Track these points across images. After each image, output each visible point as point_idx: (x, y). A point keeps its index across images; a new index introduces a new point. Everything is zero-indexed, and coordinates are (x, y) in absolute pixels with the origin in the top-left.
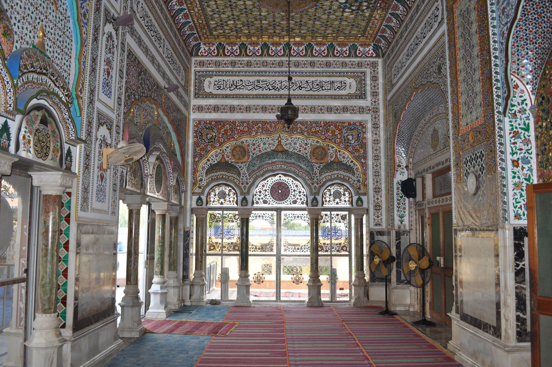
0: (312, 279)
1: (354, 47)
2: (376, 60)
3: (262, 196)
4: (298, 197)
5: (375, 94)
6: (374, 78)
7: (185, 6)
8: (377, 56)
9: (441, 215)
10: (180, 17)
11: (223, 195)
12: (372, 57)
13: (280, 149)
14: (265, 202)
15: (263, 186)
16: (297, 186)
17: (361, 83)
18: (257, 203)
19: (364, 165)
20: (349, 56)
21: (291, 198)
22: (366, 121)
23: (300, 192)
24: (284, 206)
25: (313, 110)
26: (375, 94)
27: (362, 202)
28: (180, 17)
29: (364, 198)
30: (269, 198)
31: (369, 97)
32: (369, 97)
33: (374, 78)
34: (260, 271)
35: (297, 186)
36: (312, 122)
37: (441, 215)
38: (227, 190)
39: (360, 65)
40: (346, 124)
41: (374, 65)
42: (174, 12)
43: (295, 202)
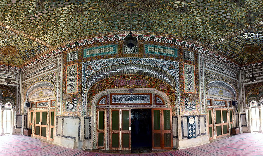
0: (171, 143)
1: (16, 68)
2: (20, 72)
5: (242, 87)
6: (19, 77)
8: (21, 71)
9: (120, 143)
11: (253, 103)
12: (19, 71)
17: (16, 77)
19: (16, 98)
20: (14, 70)
22: (17, 87)
26: (242, 87)
29: (15, 106)
31: (244, 86)
32: (244, 86)
33: (19, 77)
34: (2, 111)
37: (120, 143)
38: (254, 101)
39: (16, 72)
41: (20, 73)
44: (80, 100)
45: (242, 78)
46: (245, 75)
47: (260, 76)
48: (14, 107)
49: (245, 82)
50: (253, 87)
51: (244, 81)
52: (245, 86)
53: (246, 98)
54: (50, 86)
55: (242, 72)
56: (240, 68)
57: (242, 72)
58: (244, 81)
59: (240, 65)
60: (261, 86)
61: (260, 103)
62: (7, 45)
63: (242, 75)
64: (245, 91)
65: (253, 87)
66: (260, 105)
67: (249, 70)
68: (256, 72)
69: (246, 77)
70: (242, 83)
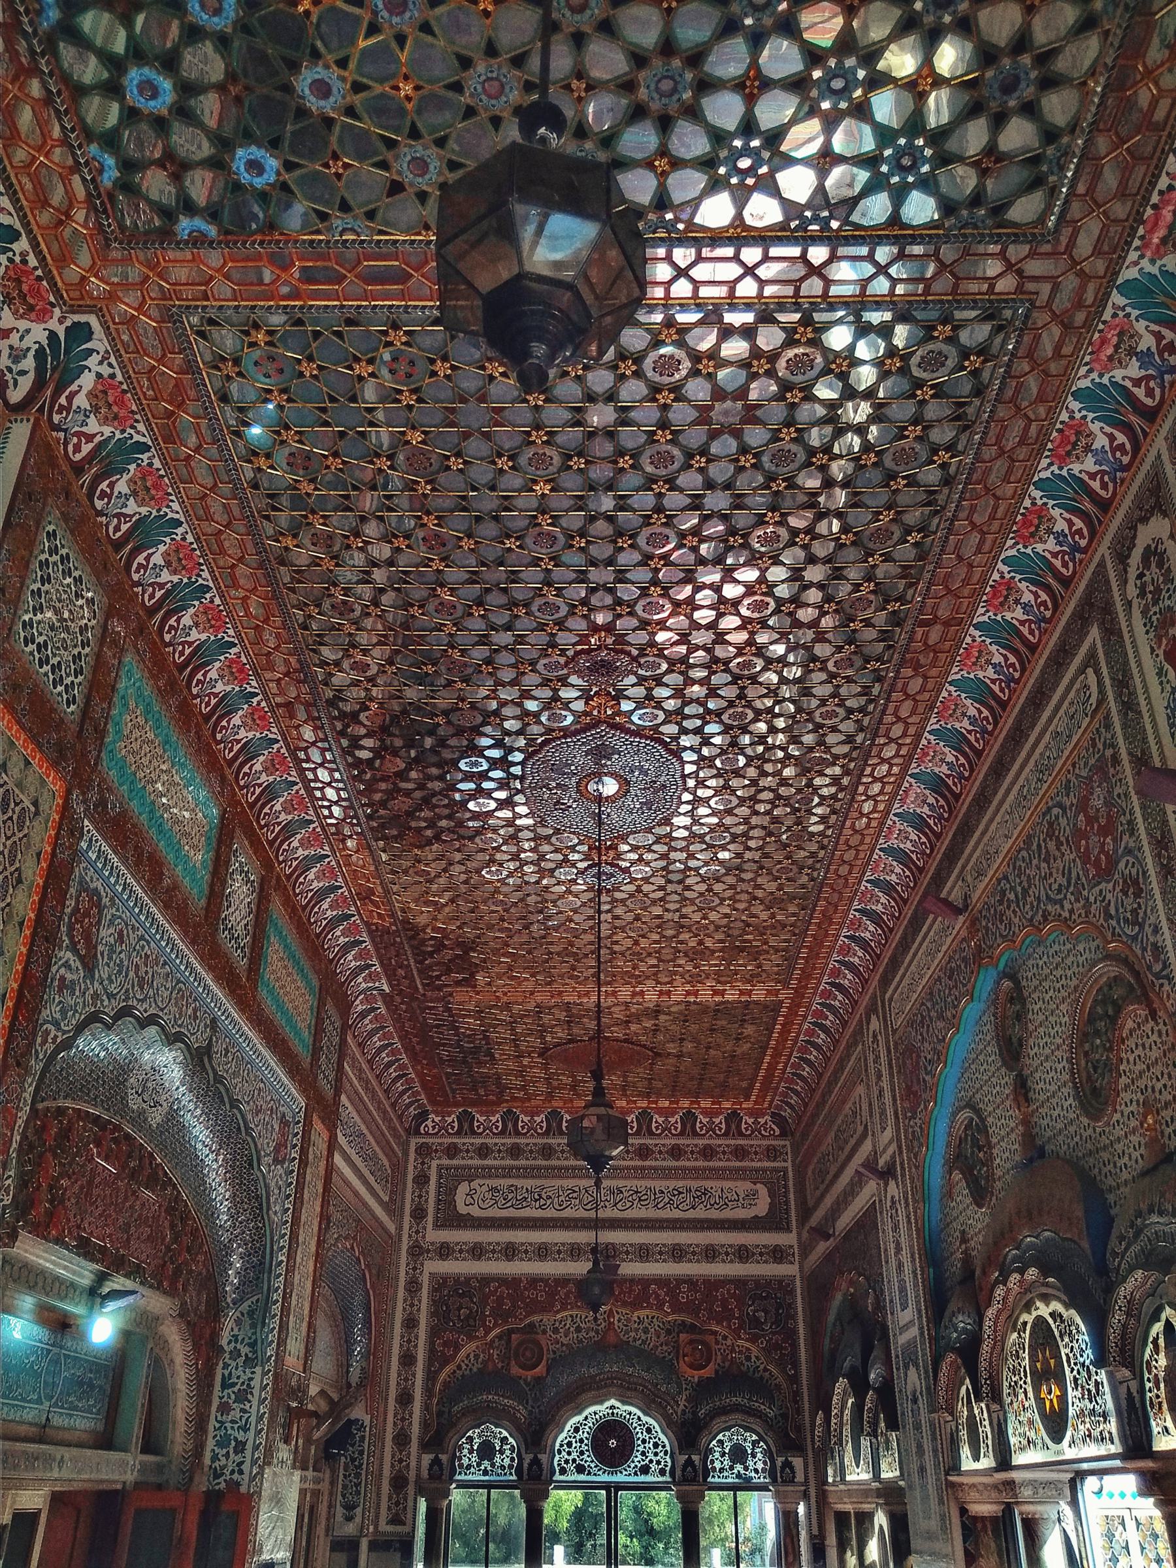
3: (574, 1455)
4: (651, 1456)
5: (413, 1286)
7: (175, 510)
10: (278, 807)
13: (612, 1338)
14: (580, 1469)
15: (577, 1430)
16: (649, 1431)
18: (563, 1471)
21: (637, 1460)
23: (656, 1445)
24: (620, 1478)
25: (644, 1253)
26: (413, 1286)
27: (792, 1468)
28: (278, 807)
29: (798, 1462)
30: (588, 1459)
31: (425, 1280)
35: (649, 1431)
36: (681, 1280)
40: (751, 1285)
42: (236, 748)
43: (645, 1470)
44: (76, 1316)
45: (419, 1214)
46: (450, 1182)
47: (647, 1228)
48: (787, 1464)
49: (445, 1251)
50: (500, 1301)
51: (435, 1236)
52: (441, 1283)
53: (428, 1391)
54: (271, 992)
55: (424, 1151)
56: (422, 1116)
57: (424, 1151)
58: (435, 1236)
59: (440, 1098)
60: (564, 1309)
61: (544, 1458)
62: (868, 144)
63: (422, 1180)
64: (434, 1333)
65: (500, 1301)
66: (446, 1472)
67: (483, 1151)
68: (539, 1182)
69: (452, 1203)
70: (417, 1251)
